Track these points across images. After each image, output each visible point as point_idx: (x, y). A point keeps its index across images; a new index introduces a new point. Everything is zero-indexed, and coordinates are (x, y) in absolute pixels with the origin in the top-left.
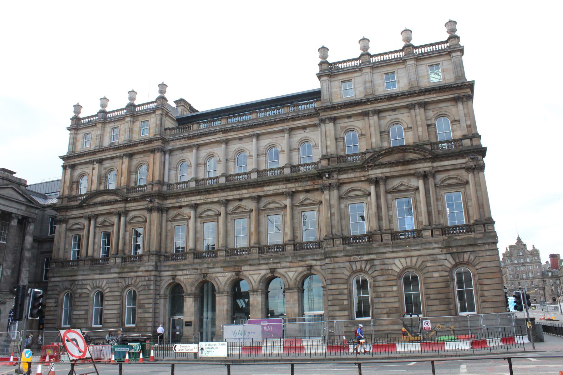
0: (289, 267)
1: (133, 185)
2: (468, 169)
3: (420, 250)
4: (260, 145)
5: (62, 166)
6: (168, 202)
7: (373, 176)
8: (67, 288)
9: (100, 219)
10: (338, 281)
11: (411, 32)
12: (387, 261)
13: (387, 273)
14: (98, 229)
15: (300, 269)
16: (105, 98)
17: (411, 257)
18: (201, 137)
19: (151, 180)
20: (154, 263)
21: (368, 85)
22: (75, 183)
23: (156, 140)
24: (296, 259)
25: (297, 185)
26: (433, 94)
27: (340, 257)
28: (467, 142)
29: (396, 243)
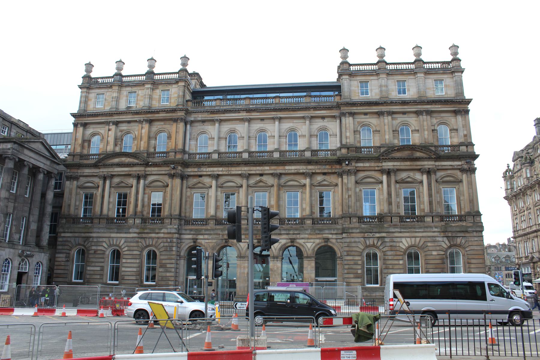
0: (308, 239)
1: (152, 150)
2: (462, 170)
3: (423, 232)
4: (281, 127)
5: (73, 123)
6: (189, 170)
7: (386, 167)
8: (79, 244)
9: (116, 180)
10: (353, 253)
11: (385, 49)
12: (395, 240)
13: (396, 249)
14: (113, 189)
15: (318, 241)
16: (121, 61)
17: (415, 237)
18: (224, 113)
19: (174, 148)
20: (176, 227)
21: (384, 88)
22: (87, 142)
23: (180, 110)
24: (315, 232)
25: (316, 167)
26: (438, 105)
27: (356, 233)
28: (463, 149)
29: (403, 225)
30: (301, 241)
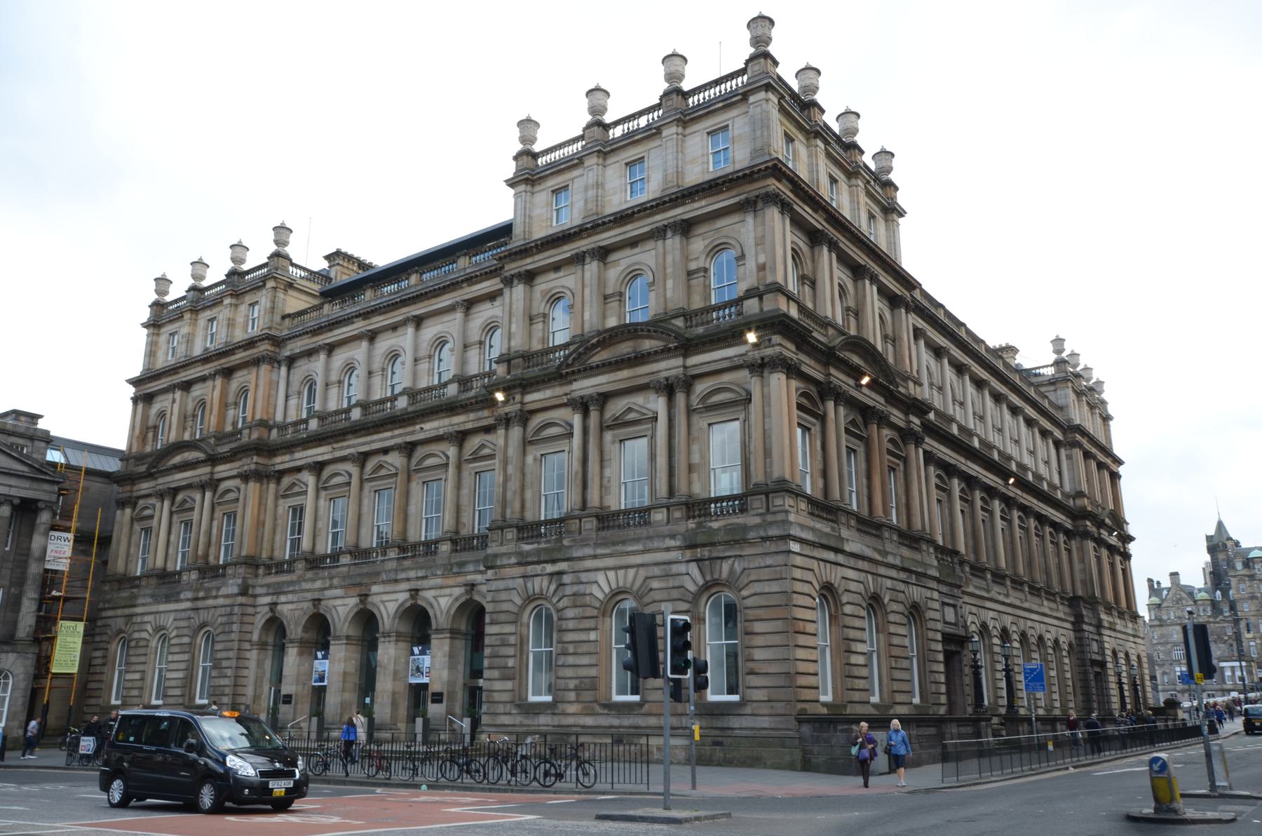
0: (441, 587)
6: (278, 460)
10: (503, 617)
12: (584, 577)
18: (331, 330)
26: (700, 199)
30: (429, 594)
